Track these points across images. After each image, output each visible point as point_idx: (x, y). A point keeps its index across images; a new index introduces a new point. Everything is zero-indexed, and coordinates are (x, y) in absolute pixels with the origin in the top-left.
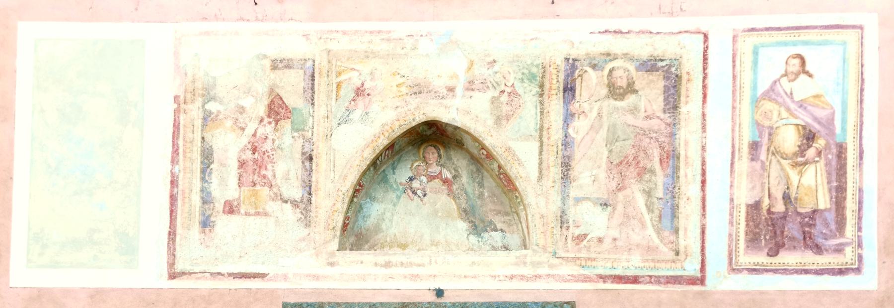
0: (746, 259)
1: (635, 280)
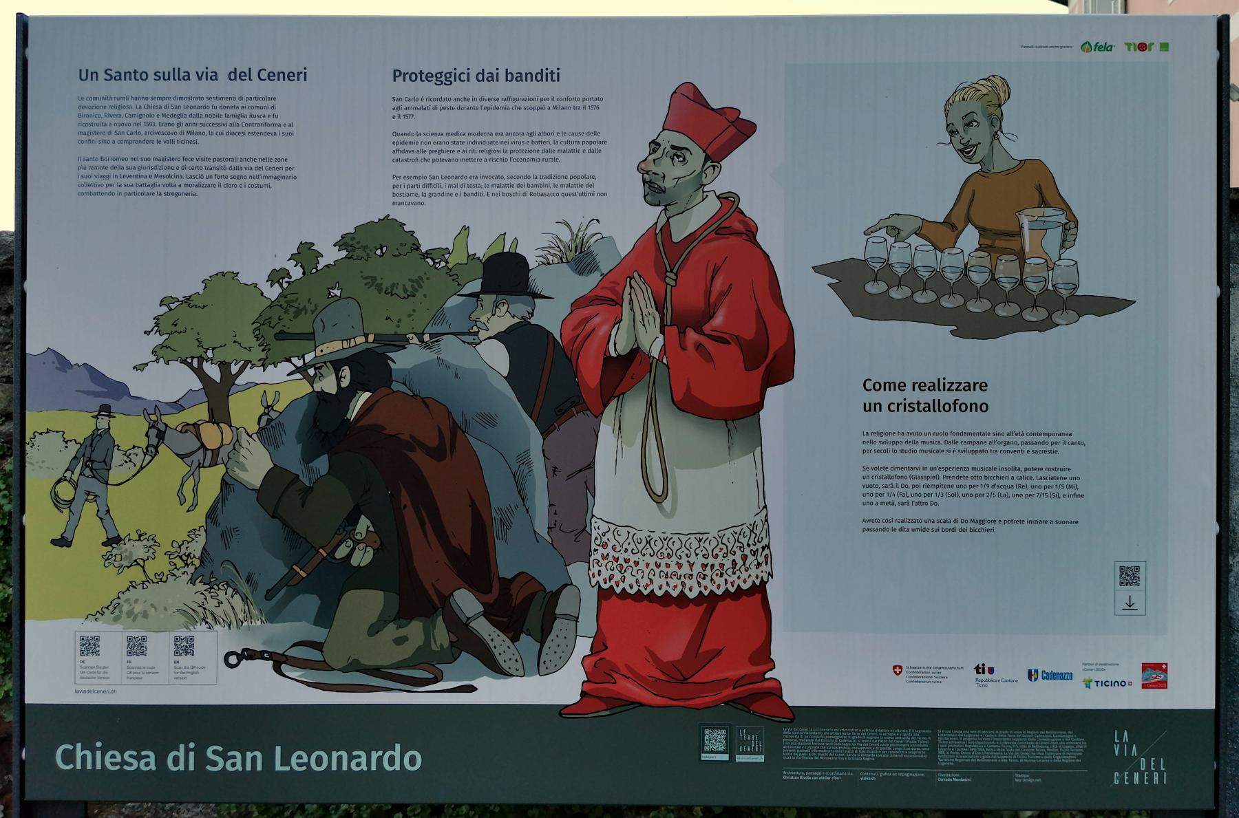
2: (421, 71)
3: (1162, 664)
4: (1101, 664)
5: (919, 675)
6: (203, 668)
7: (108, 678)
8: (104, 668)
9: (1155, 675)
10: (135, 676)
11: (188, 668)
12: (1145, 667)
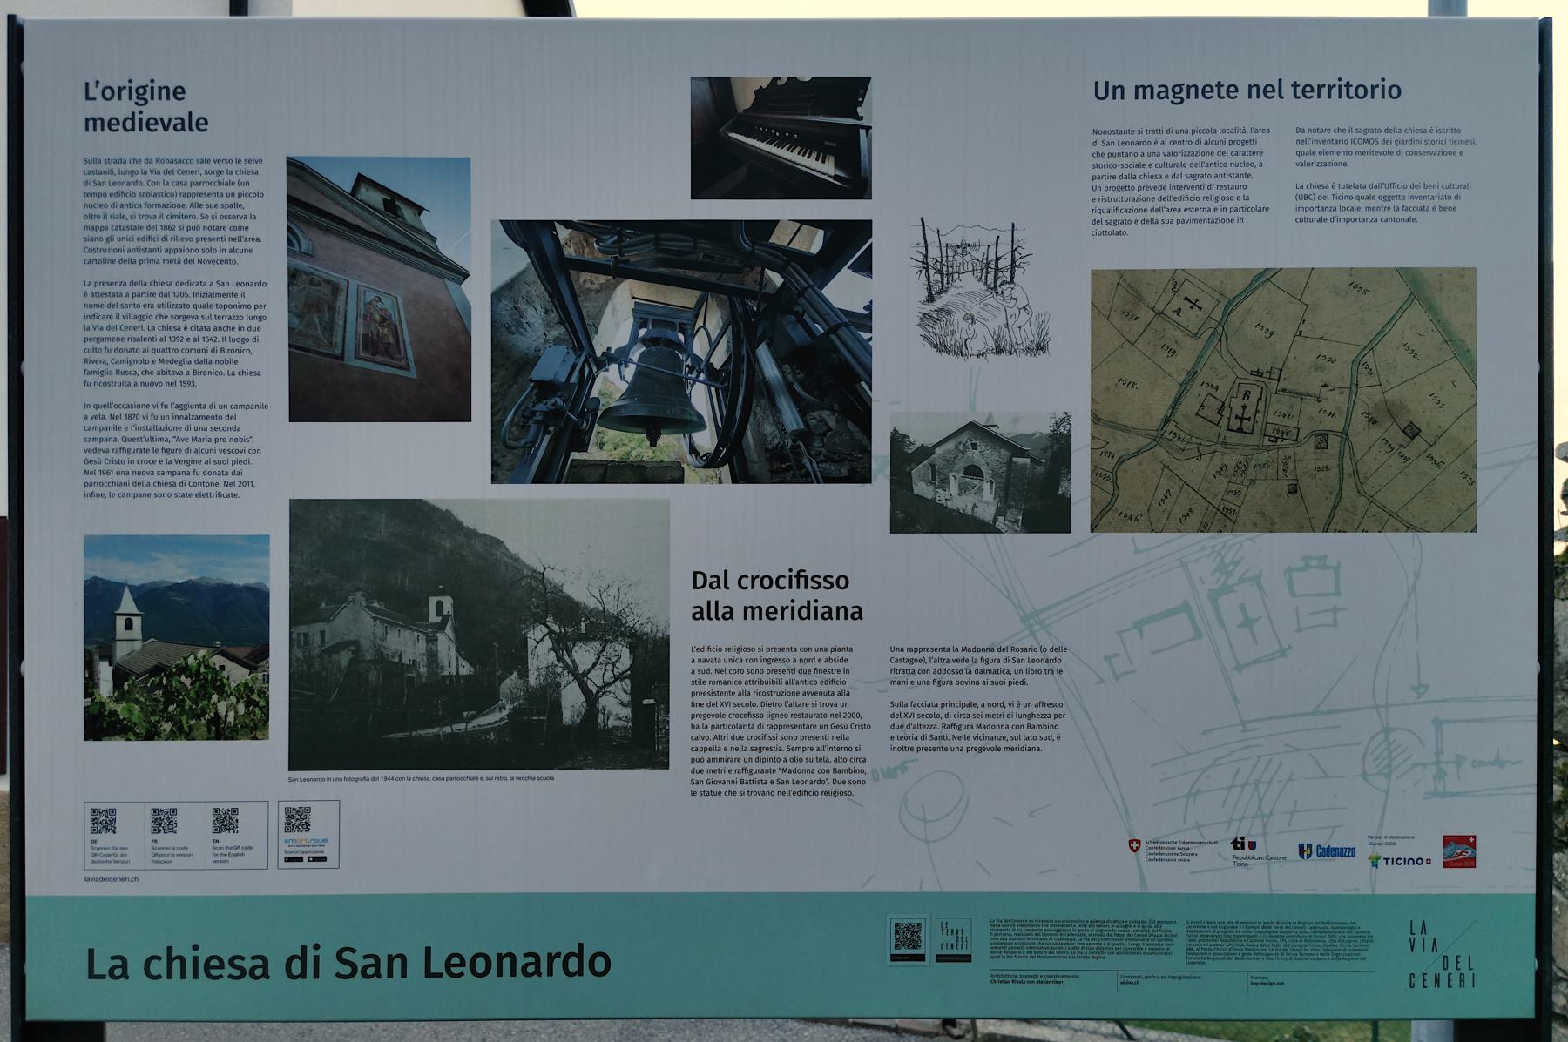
0: (362, 354)
2: (1219, 83)
3: (1469, 837)
4: (1391, 837)
5: (1162, 851)
6: (250, 848)
7: (127, 862)
8: (122, 849)
9: (1460, 852)
10: (163, 859)
11: (231, 848)
12: (1448, 840)
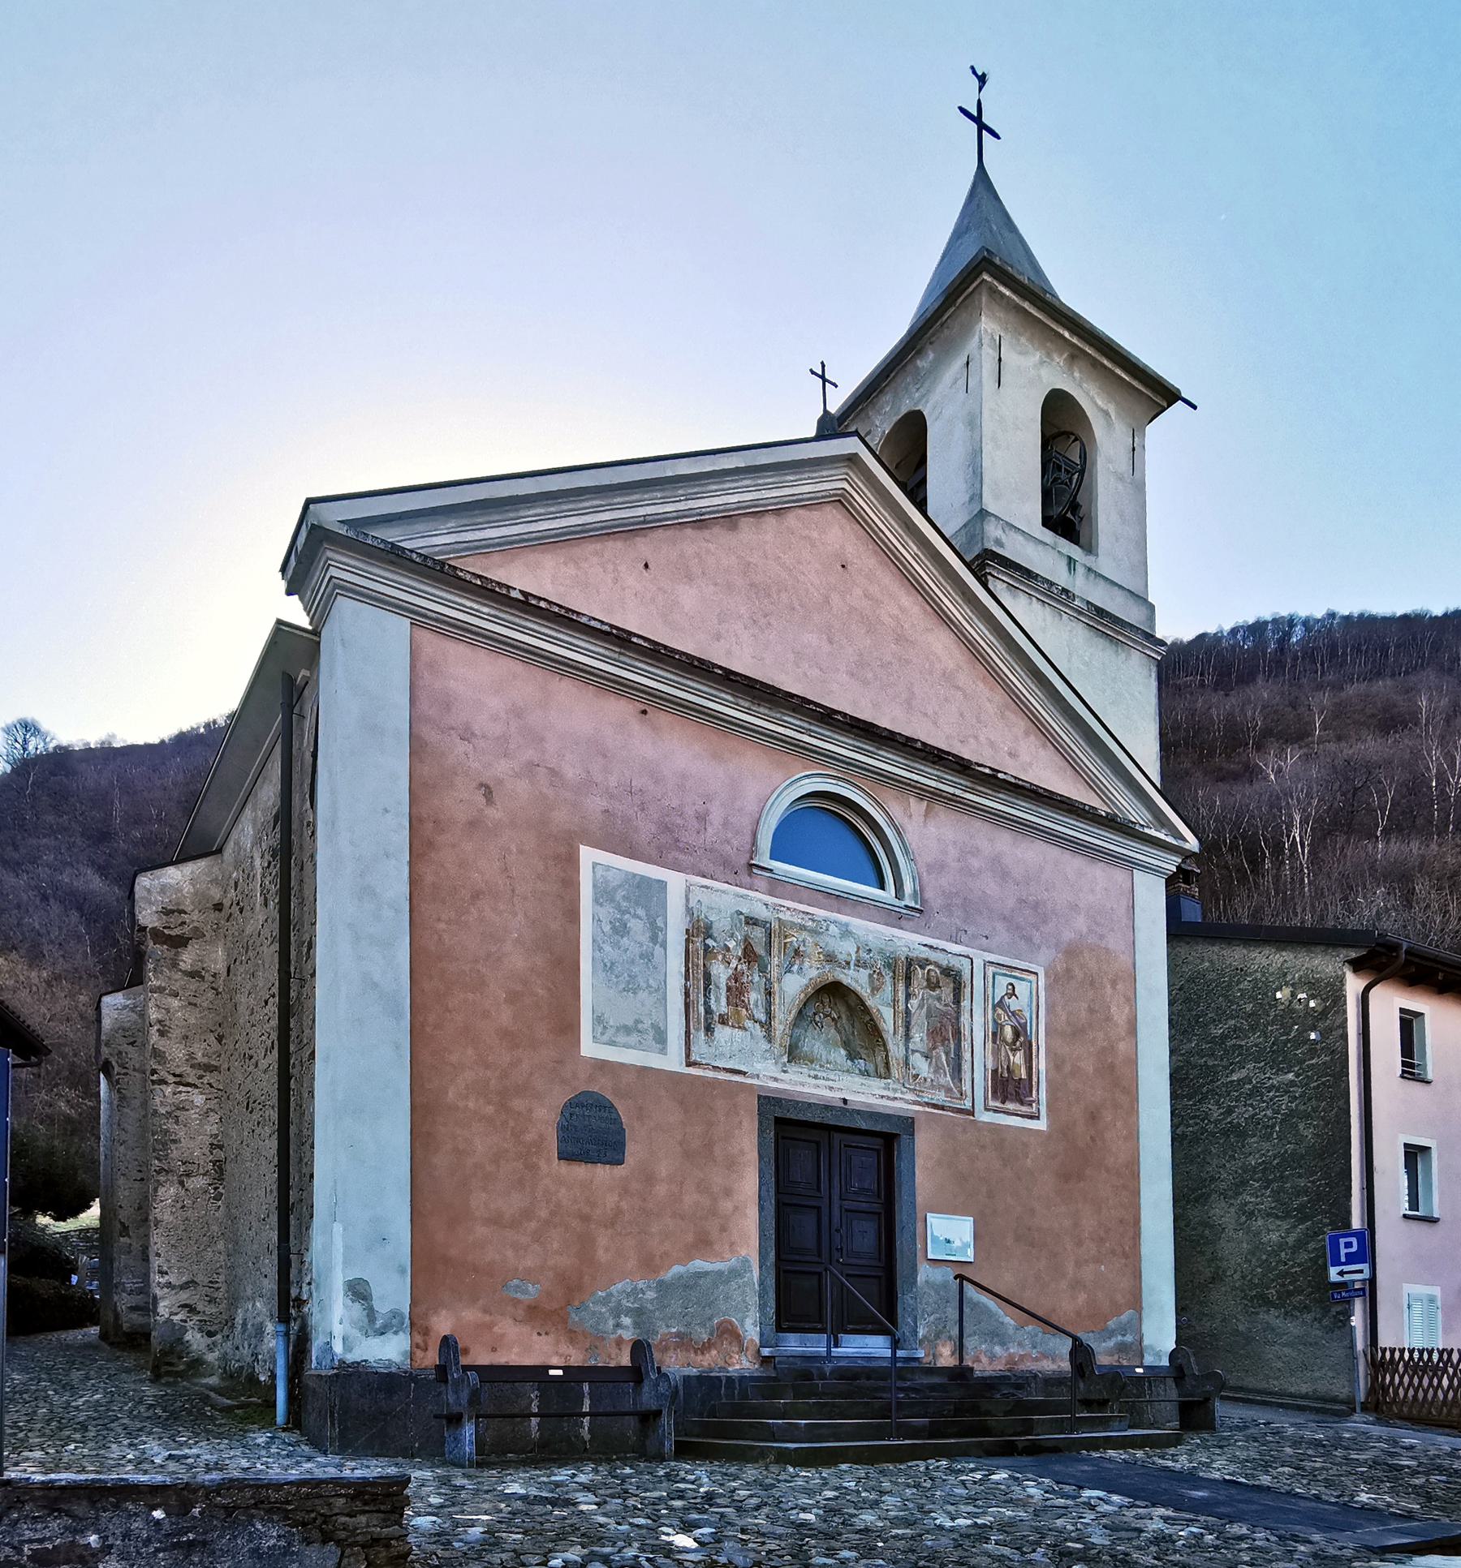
0: (992, 1103)
1: (942, 1108)
